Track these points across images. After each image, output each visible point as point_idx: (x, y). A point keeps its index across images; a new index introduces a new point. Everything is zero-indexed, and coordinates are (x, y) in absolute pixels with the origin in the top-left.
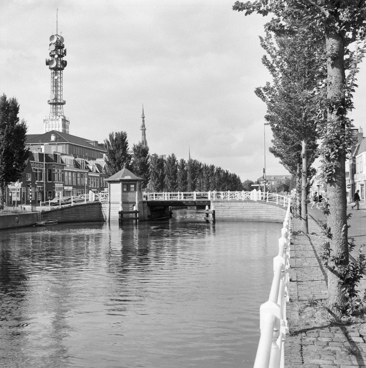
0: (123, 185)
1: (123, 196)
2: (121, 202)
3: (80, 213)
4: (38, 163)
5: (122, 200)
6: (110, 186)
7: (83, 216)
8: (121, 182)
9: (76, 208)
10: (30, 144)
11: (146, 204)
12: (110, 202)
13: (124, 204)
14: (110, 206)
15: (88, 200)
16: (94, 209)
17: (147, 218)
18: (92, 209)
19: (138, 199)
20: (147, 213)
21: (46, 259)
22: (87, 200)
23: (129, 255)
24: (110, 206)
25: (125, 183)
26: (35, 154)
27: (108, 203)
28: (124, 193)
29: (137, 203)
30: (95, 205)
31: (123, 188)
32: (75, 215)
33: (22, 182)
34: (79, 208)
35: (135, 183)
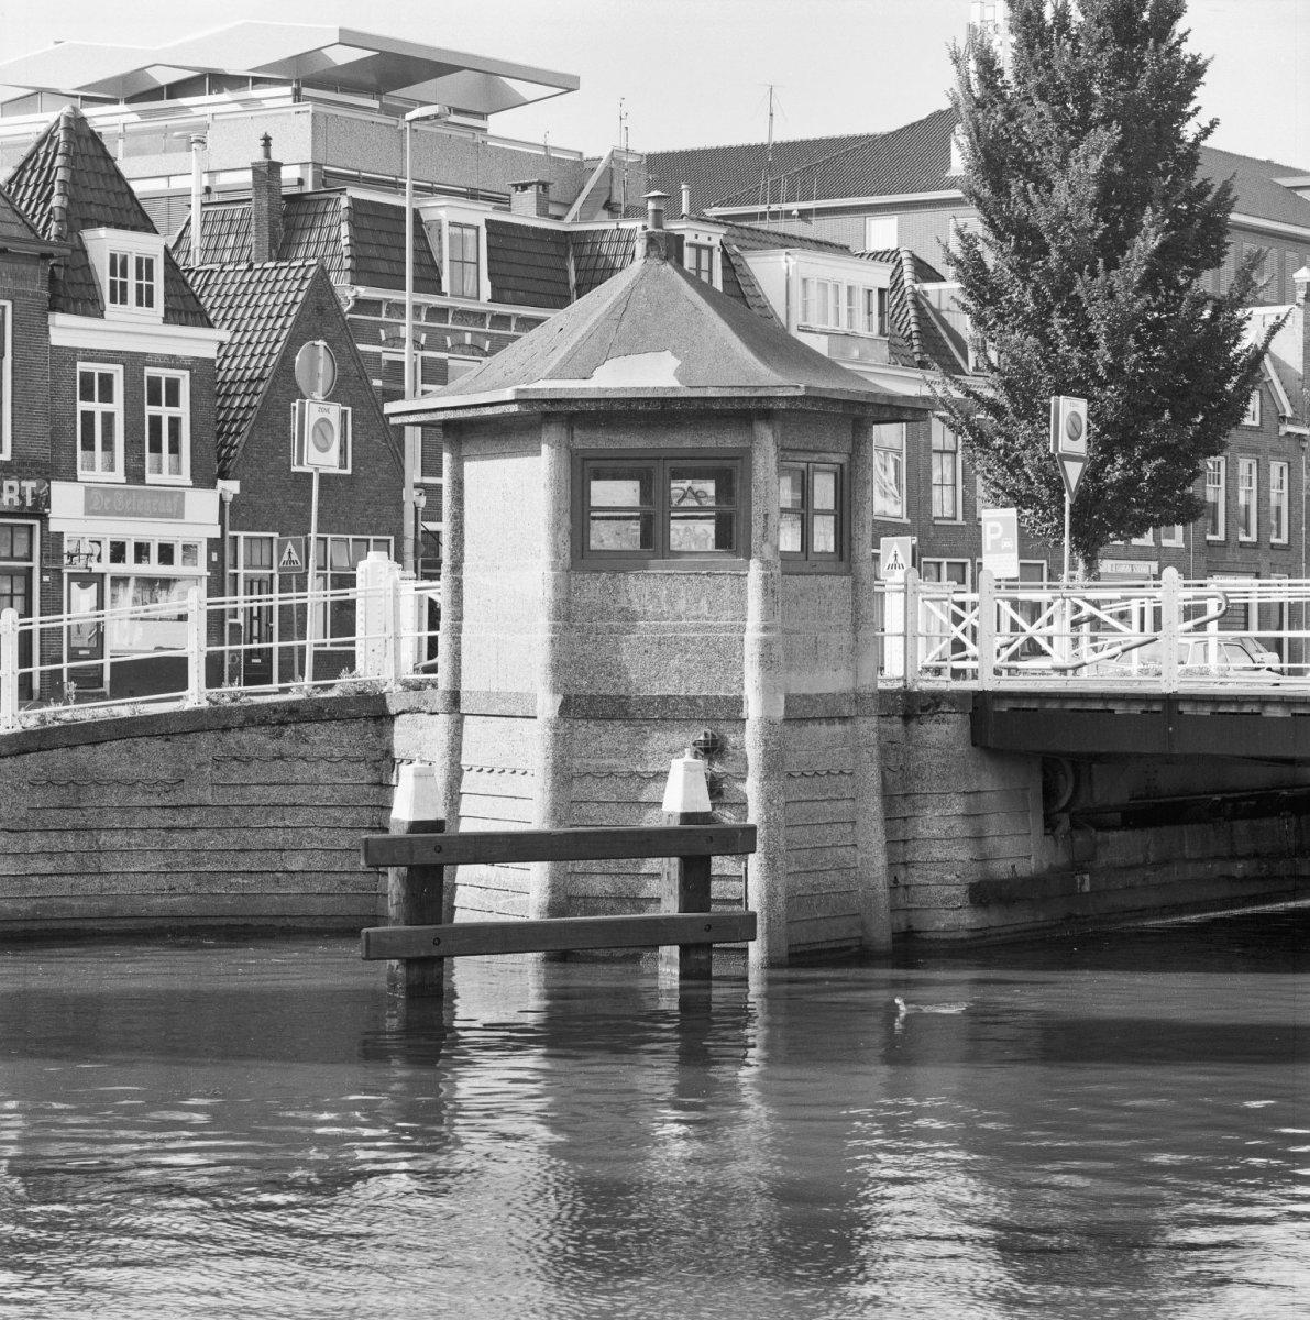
0: (581, 472)
1: (566, 614)
2: (547, 704)
3: (115, 819)
4: (480, 317)
5: (564, 666)
6: (458, 484)
7: (155, 863)
8: (554, 433)
9: (60, 758)
10: (795, 207)
11: (945, 733)
12: (455, 698)
13: (585, 729)
14: (455, 749)
15: (347, 660)
16: (302, 771)
17: (953, 917)
18: (278, 771)
19: (767, 661)
20: (963, 854)
21: (203, 1262)
22: (335, 663)
23: (1187, 1223)
24: (455, 749)
25: (601, 441)
26: (446, 231)
27: (440, 705)
28: (593, 588)
29: (753, 709)
30: (319, 734)
31: (577, 515)
32: (36, 842)
33: (231, 487)
34: (103, 757)
35: (729, 440)
